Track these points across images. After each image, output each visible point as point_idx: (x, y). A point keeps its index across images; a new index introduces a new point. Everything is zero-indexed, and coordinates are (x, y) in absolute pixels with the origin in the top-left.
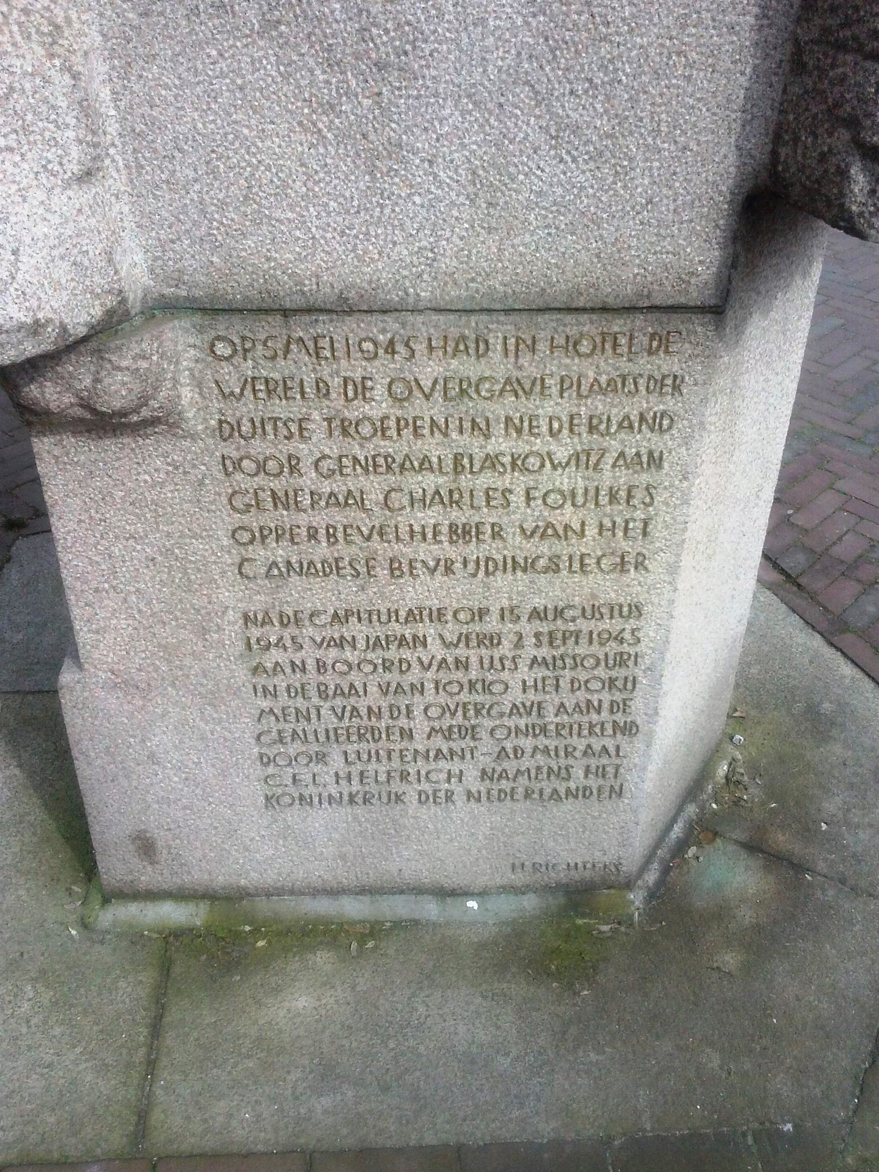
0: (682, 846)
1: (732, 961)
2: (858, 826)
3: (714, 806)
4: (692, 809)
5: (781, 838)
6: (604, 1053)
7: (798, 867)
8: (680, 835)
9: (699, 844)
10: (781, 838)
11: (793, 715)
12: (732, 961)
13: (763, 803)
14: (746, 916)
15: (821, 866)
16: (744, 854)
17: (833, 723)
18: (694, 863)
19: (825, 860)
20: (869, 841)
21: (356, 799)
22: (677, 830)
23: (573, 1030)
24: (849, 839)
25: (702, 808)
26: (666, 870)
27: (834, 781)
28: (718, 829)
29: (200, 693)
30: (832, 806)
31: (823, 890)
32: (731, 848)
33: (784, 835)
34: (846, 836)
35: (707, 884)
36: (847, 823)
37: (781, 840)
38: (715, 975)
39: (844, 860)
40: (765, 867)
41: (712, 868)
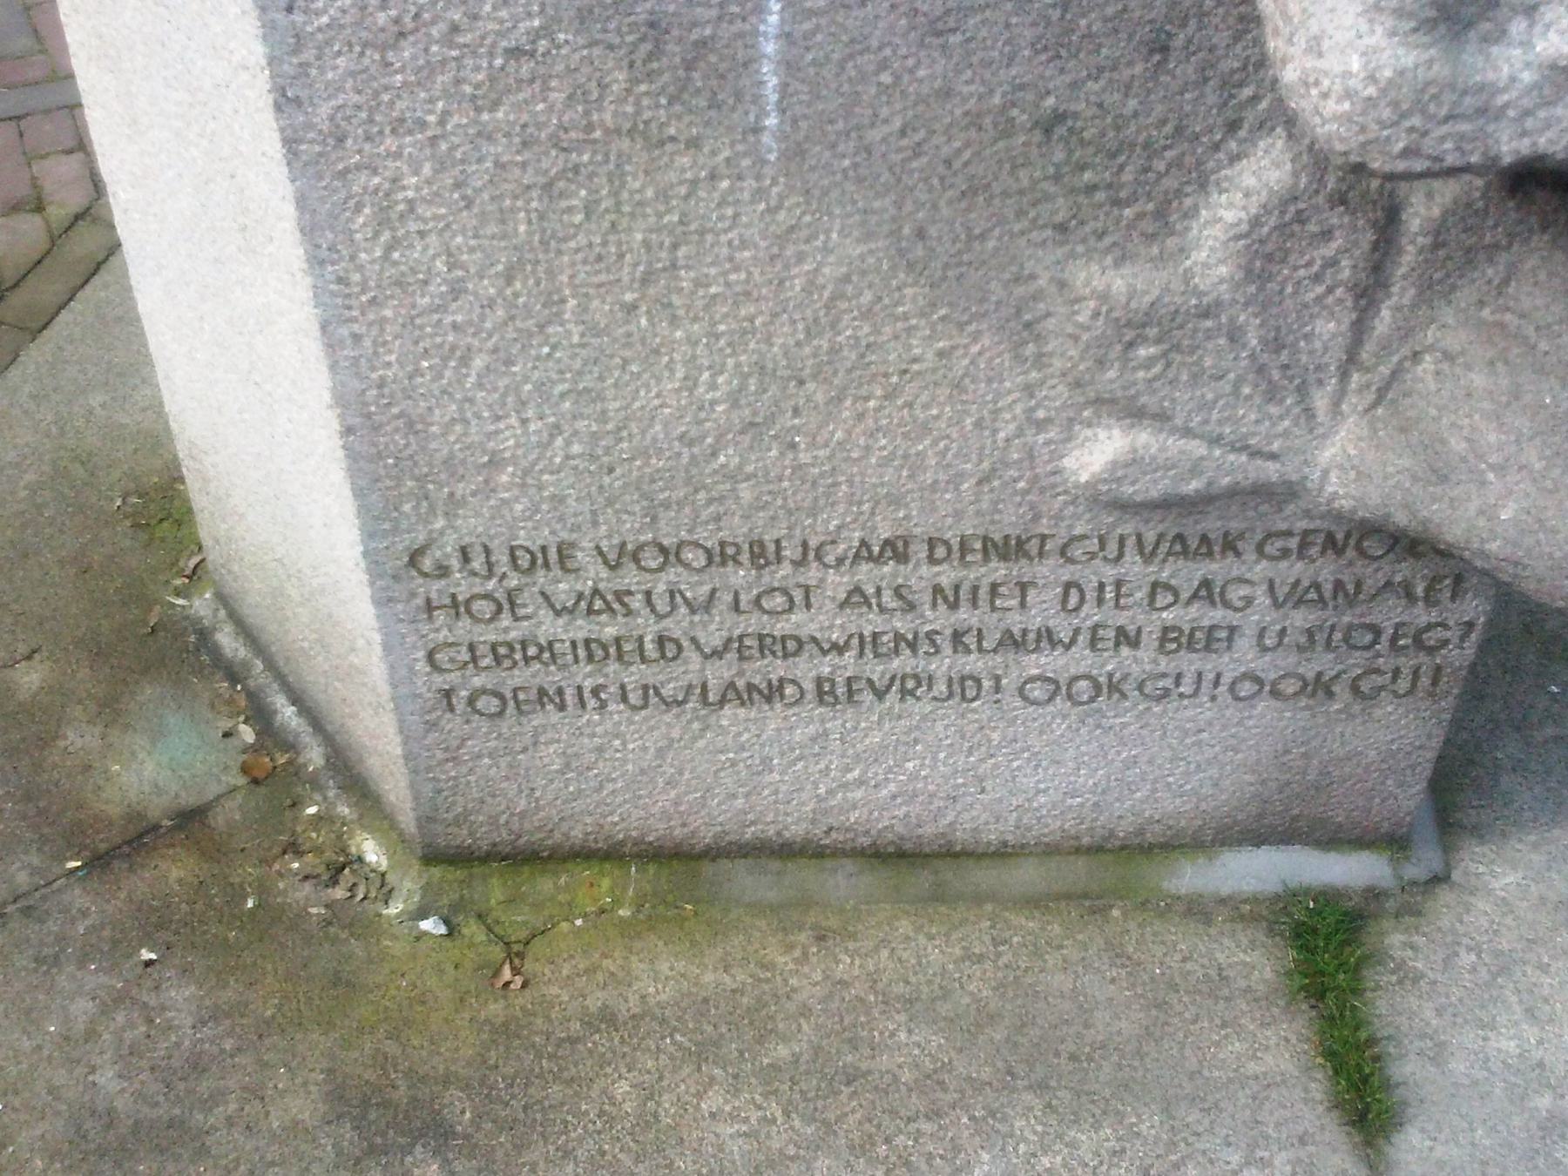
0: (260, 715)
1: (26, 679)
2: (105, 1011)
3: (312, 810)
4: (314, 756)
5: (175, 873)
6: (25, 488)
7: (99, 862)
8: (279, 717)
9: (254, 749)
10: (175, 873)
11: (446, 1082)
12: (26, 679)
13: (262, 890)
14: (79, 738)
15: (77, 897)
16: (189, 800)
17: (372, 1150)
18: (225, 724)
19: (85, 913)
20: (64, 1008)
21: (1027, 547)
22: (287, 713)
23: (79, 471)
24: (95, 978)
25: (315, 783)
26: (234, 675)
27: (228, 1045)
28: (262, 790)
29: (838, 133)
30: (180, 998)
31: (34, 871)
32: (213, 790)
33: (180, 881)
34: (104, 979)
35: (173, 720)
36: (119, 999)
37: (174, 870)
38: (22, 649)
39: (61, 939)
40: (140, 816)
41: (196, 742)
